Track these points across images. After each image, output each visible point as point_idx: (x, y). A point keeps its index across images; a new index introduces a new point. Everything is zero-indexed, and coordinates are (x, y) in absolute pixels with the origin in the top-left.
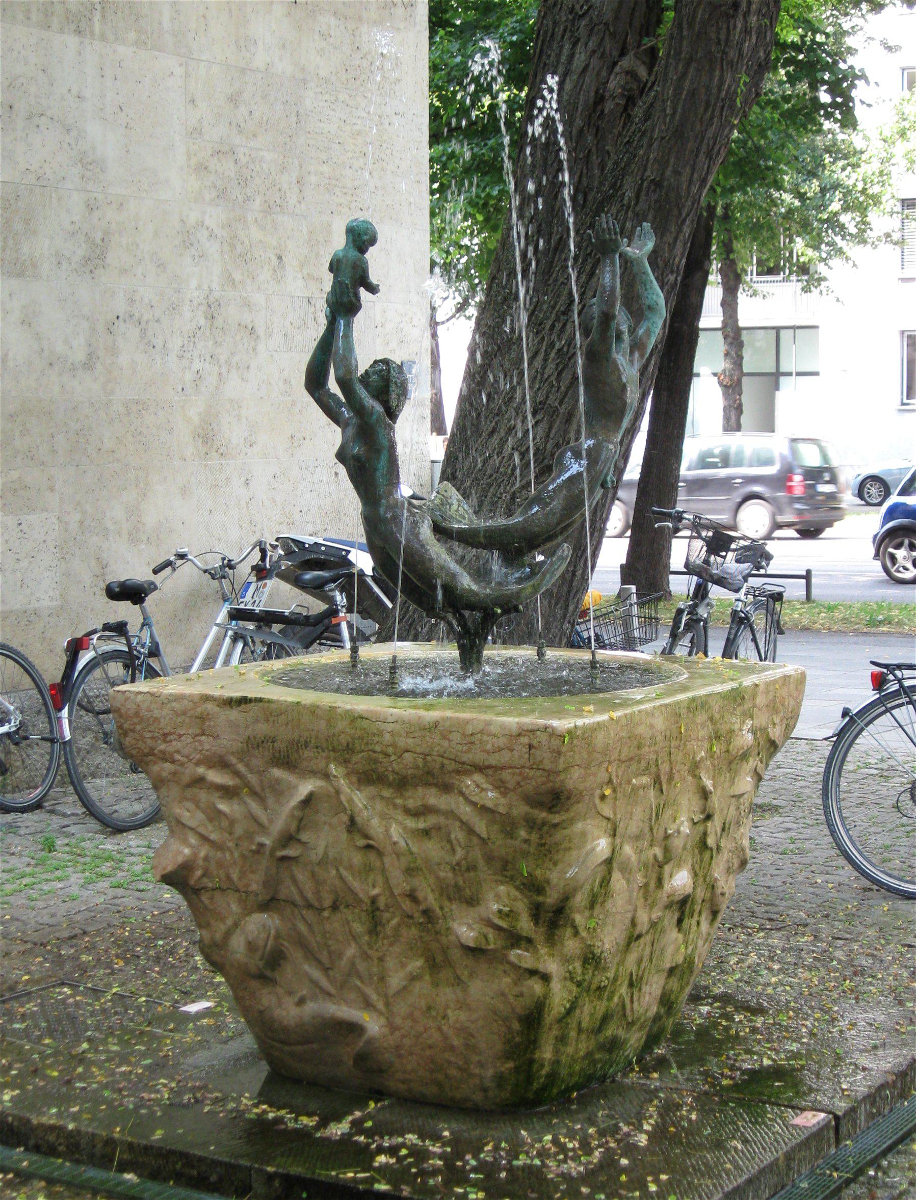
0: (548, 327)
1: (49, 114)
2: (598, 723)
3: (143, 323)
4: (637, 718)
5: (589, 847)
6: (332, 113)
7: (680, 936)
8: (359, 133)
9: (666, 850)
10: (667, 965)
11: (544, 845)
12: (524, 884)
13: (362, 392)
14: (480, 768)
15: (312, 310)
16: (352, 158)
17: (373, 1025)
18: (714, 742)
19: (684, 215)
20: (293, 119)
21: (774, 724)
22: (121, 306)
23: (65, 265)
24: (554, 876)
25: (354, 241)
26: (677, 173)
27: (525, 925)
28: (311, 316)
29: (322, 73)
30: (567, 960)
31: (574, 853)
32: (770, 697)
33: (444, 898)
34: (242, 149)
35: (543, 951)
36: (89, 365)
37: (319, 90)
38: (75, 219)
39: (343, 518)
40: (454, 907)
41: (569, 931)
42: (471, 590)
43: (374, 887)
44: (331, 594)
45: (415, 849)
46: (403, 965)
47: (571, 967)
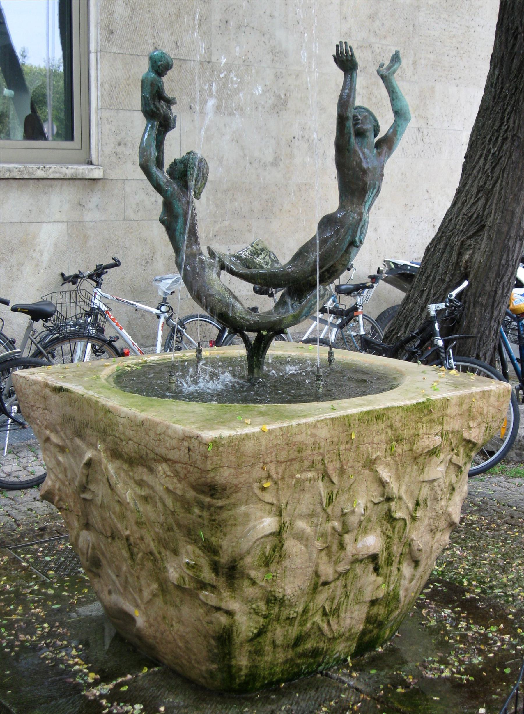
0: (488, 139)
1: (251, 25)
2: (247, 435)
3: (311, 141)
4: (295, 430)
5: (251, 524)
7: (380, 579)
8: (454, 36)
9: (344, 524)
10: (368, 599)
11: (214, 520)
12: (204, 546)
14: (166, 460)
16: (449, 50)
17: (140, 621)
18: (394, 443)
20: (411, 28)
21: (470, 428)
22: (296, 131)
23: (260, 108)
24: (225, 543)
27: (207, 575)
30: (248, 601)
31: (239, 528)
32: (465, 407)
33: (161, 546)
34: (377, 45)
35: (226, 594)
36: (275, 163)
37: (428, 12)
38: (268, 83)
40: (167, 553)
41: (246, 582)
43: (127, 529)
45: (141, 509)
46: (149, 585)
47: (254, 606)
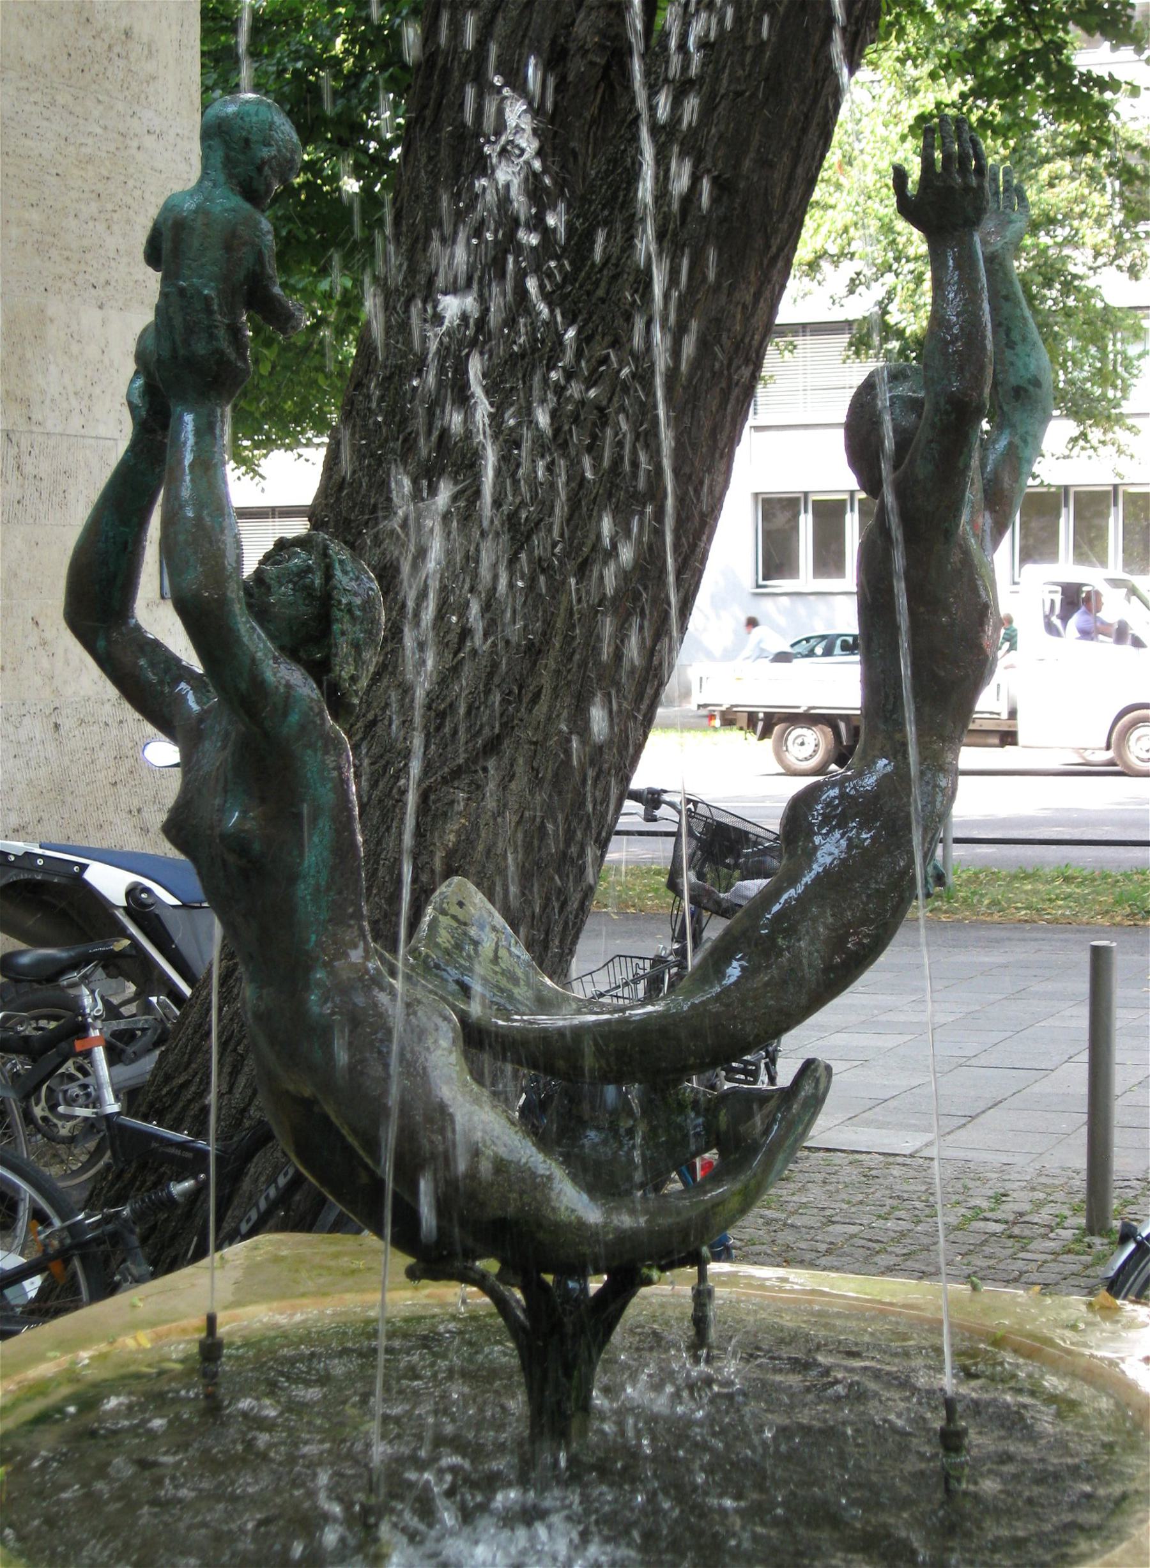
6: (45, 124)
8: (90, 160)
13: (255, 640)
15: (13, 451)
19: (774, 249)
25: (229, 163)
26: (765, 163)
28: (11, 462)
29: (29, 58)
37: (24, 84)
39: (69, 799)
42: (581, 1224)
44: (72, 992)
